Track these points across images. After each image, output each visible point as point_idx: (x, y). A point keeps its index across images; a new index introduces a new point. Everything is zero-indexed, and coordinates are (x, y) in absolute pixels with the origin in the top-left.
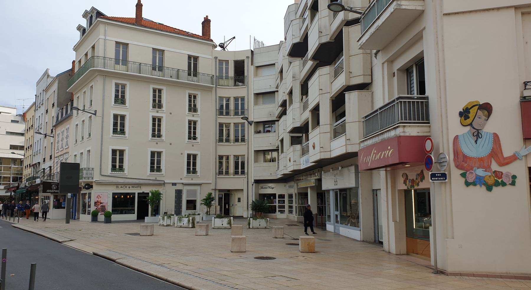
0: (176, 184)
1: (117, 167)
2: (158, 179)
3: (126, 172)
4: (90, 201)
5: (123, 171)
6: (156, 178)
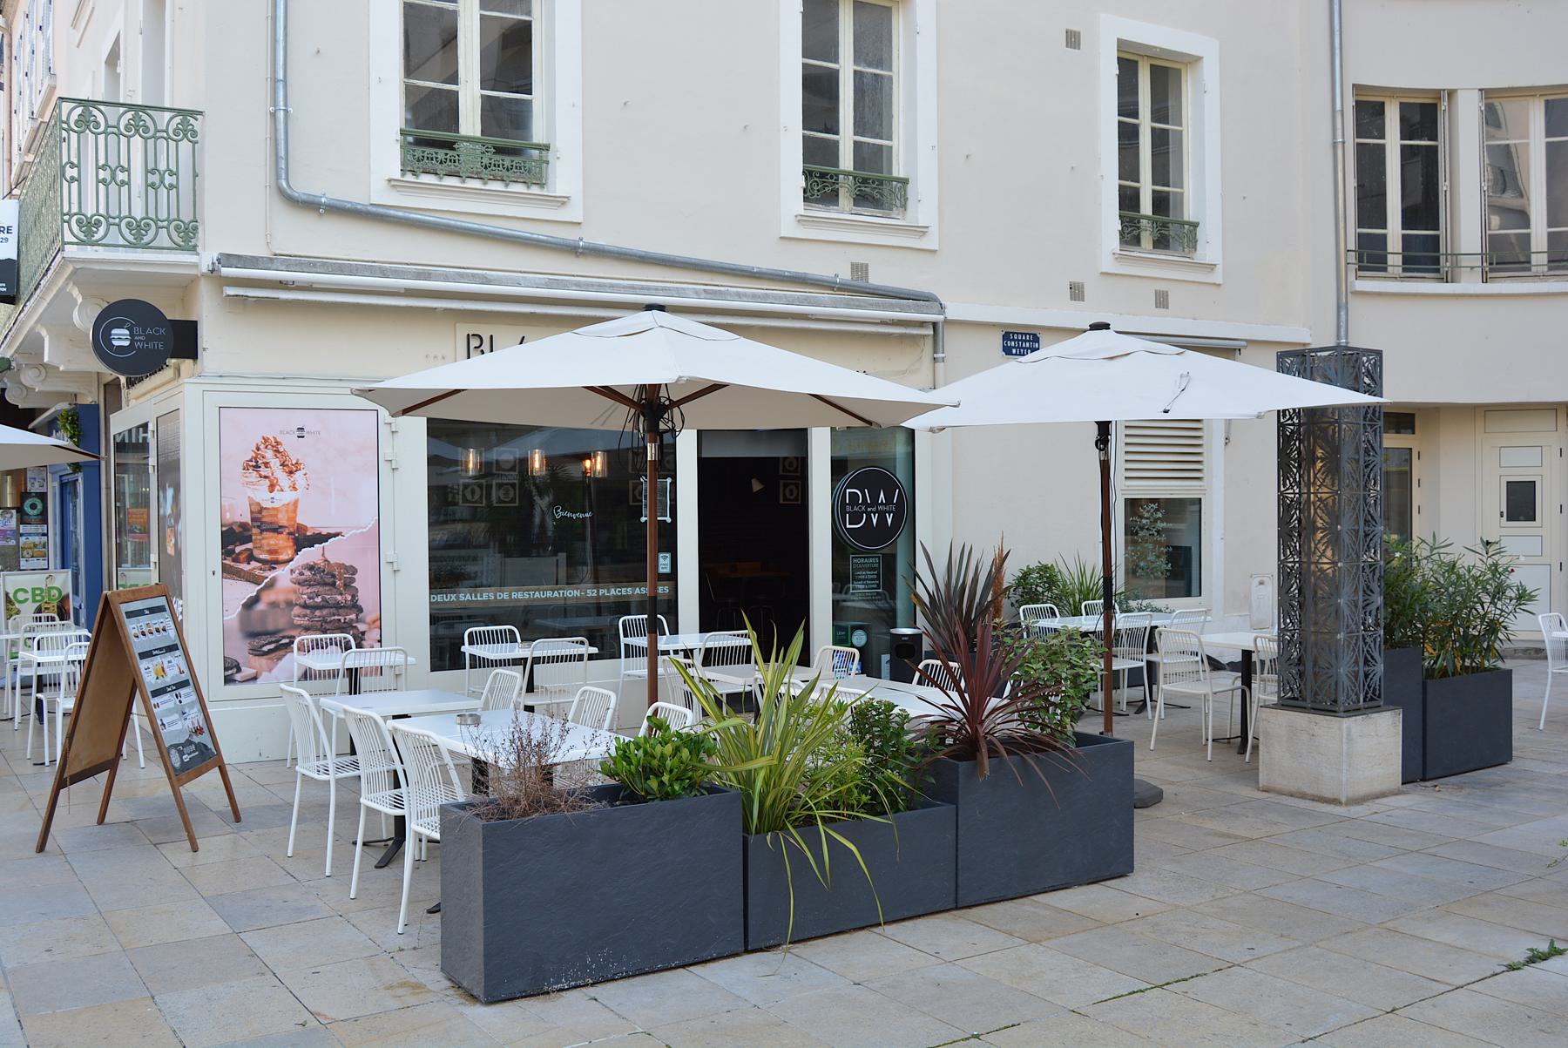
0: (1036, 339)
1: (470, 122)
2: (876, 279)
3: (565, 175)
4: (177, 515)
5: (535, 177)
6: (859, 269)
